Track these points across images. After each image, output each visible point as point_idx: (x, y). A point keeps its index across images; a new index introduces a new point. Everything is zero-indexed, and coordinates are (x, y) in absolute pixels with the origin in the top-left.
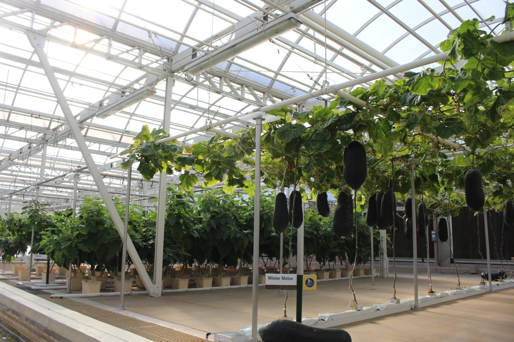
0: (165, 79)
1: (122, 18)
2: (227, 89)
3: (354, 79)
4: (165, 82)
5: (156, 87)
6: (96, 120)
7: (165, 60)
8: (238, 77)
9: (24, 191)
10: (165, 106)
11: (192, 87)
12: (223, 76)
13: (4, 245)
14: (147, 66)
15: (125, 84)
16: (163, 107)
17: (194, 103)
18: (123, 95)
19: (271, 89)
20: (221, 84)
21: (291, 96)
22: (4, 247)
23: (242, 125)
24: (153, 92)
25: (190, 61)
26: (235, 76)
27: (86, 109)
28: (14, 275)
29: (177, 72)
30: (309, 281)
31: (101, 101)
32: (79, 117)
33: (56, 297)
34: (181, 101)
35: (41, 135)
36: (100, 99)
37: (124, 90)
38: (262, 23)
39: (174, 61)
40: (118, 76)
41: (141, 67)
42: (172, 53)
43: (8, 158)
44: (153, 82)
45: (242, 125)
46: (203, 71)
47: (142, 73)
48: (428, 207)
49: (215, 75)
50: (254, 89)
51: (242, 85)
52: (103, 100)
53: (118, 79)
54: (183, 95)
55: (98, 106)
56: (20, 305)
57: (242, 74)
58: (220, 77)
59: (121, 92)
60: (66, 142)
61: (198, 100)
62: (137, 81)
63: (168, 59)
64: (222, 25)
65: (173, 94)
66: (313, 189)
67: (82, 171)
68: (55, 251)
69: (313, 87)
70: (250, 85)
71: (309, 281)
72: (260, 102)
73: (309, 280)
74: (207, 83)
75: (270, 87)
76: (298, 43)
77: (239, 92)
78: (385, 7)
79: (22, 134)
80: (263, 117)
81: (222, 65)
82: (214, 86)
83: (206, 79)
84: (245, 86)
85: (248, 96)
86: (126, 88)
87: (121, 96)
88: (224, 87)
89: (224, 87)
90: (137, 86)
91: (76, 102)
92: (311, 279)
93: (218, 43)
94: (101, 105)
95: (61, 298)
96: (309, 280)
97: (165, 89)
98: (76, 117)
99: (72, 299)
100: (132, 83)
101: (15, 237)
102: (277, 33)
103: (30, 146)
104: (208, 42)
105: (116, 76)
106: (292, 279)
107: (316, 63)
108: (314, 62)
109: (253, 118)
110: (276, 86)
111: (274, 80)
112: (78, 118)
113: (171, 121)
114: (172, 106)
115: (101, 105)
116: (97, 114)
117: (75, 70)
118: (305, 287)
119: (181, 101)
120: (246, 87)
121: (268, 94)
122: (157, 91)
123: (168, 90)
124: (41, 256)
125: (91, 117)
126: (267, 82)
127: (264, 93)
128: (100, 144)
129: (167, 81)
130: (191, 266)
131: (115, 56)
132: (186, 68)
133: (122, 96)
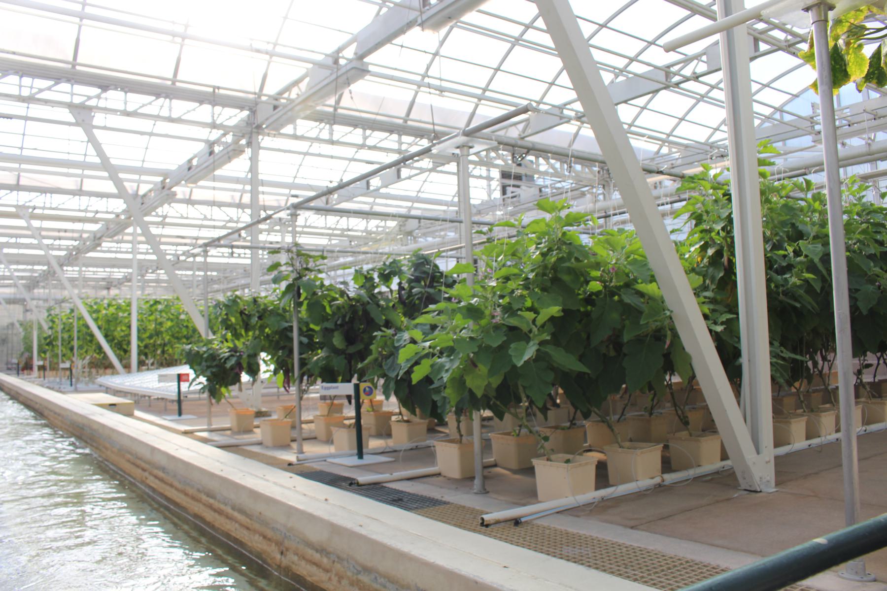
9: (236, 235)
13: (209, 364)
22: (208, 367)
28: (236, 430)
30: (367, 389)
32: (196, 159)
33: (498, 522)
35: (246, 113)
43: (160, 186)
56: (255, 495)
60: (295, 129)
67: (303, 206)
68: (466, 377)
71: (367, 389)
79: (204, 112)
80: (470, 145)
87: (272, 107)
92: (369, 387)
95: (517, 522)
99: (544, 522)
101: (98, 356)
102: (450, 18)
103: (190, 165)
109: (803, 5)
124: (337, 388)
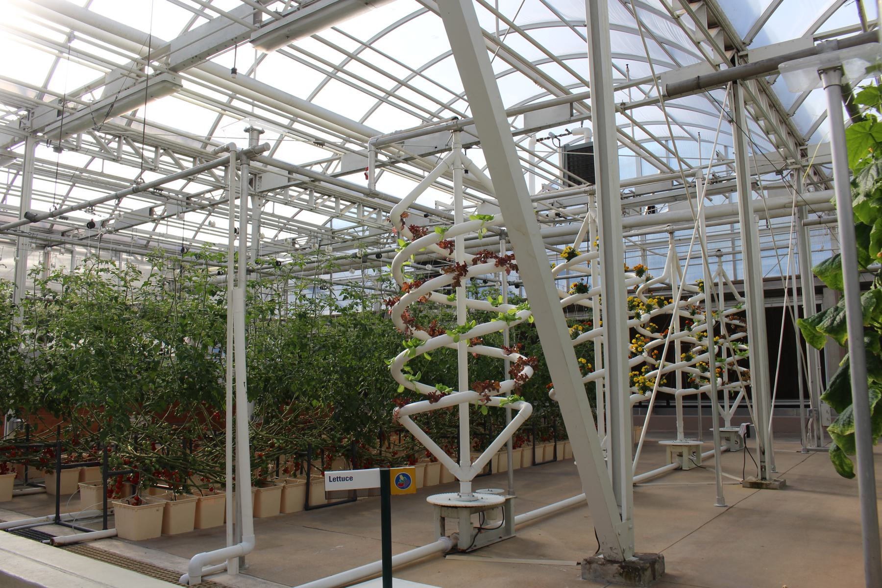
0: (24, 142)
4: (24, 146)
10: (22, 196)
12: (122, 135)
16: (19, 199)
30: (402, 478)
38: (134, 81)
44: (8, 144)
48: (840, 433)
64: (95, 74)
66: (428, 358)
71: (402, 478)
73: (401, 477)
81: (119, 121)
92: (404, 475)
93: (86, 98)
96: (401, 477)
102: (367, 4)
104: (76, 95)
116: (254, 36)
118: (395, 489)
128: (91, 92)
129: (26, 144)
130: (143, 439)
132: (47, 129)
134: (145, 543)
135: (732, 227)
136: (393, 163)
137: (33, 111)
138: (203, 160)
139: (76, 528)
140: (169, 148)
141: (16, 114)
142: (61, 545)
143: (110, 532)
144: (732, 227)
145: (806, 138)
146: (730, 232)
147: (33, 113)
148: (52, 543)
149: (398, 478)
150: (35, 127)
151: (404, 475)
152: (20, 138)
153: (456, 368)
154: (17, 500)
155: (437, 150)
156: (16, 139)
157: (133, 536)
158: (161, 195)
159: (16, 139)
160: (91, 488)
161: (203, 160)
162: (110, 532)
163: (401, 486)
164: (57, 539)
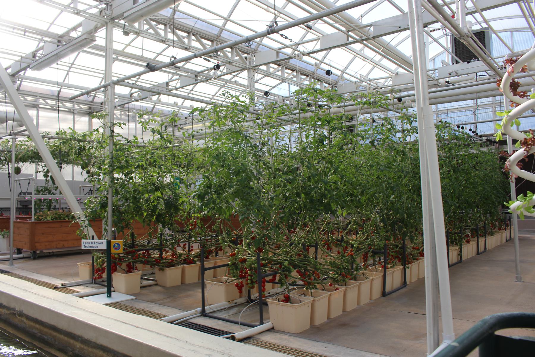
0: (105, 27)
1: (227, 27)
2: (171, 36)
3: (292, 20)
5: (95, 35)
6: (30, 73)
7: (104, 6)
8: (194, 28)
11: (135, 36)
14: (84, 12)
15: (60, 31)
17: (139, 53)
18: (59, 44)
19: (220, 38)
20: (165, 30)
21: (227, 41)
23: (53, 40)
24: (93, 40)
25: (132, 7)
26: (192, 27)
27: (16, 61)
29: (117, 19)
30: (116, 245)
31: (34, 52)
34: (156, 59)
36: (33, 49)
37: (60, 39)
39: (113, 7)
40: (53, 22)
41: (78, 13)
42: (215, 36)
45: (53, 40)
46: (147, 18)
47: (79, 19)
49: (159, 23)
50: (202, 38)
51: (189, 33)
52: (37, 51)
53: (53, 25)
54: (159, 52)
55: (31, 57)
57: (190, 23)
58: (165, 25)
59: (56, 41)
61: (143, 49)
62: (75, 29)
63: (107, 4)
65: (114, 42)
69: (322, 61)
70: (197, 32)
71: (116, 245)
72: (184, 43)
74: (151, 31)
75: (219, 36)
76: (284, 9)
77: (186, 41)
78: (435, 38)
82: (157, 33)
83: (151, 27)
84: (191, 34)
85: (195, 44)
86: (61, 36)
88: (193, 42)
89: (193, 42)
90: (74, 34)
91: (7, 53)
92: (117, 244)
94: (34, 56)
97: (105, 37)
98: (6, 69)
100: (68, 33)
105: (51, 22)
106: (102, 243)
107: (268, 12)
108: (266, 10)
110: (225, 35)
111: (222, 29)
112: (9, 71)
113: (113, 72)
114: (114, 56)
115: (34, 56)
117: (48, 29)
119: (156, 59)
120: (194, 35)
121: (236, 49)
122: (97, 38)
123: (109, 38)
125: (25, 69)
126: (215, 31)
127: (212, 41)
129: (107, 29)
131: (82, 11)
133: (58, 46)
134: (303, 334)
135: (437, 107)
136: (207, 80)
137: (111, 4)
138: (218, 43)
139: (242, 324)
140: (200, 35)
141: (96, 7)
142: (241, 341)
143: (267, 325)
144: (437, 107)
145: (337, 81)
146: (472, 105)
147: (111, 5)
148: (233, 338)
149: (114, 245)
150: (114, 15)
151: (117, 244)
152: (102, 24)
153: (417, 190)
154: (144, 291)
155: (400, 29)
156: (99, 25)
157: (293, 330)
158: (187, 72)
159: (99, 25)
160: (219, 285)
161: (218, 43)
162: (267, 325)
163: (116, 249)
164: (237, 335)
